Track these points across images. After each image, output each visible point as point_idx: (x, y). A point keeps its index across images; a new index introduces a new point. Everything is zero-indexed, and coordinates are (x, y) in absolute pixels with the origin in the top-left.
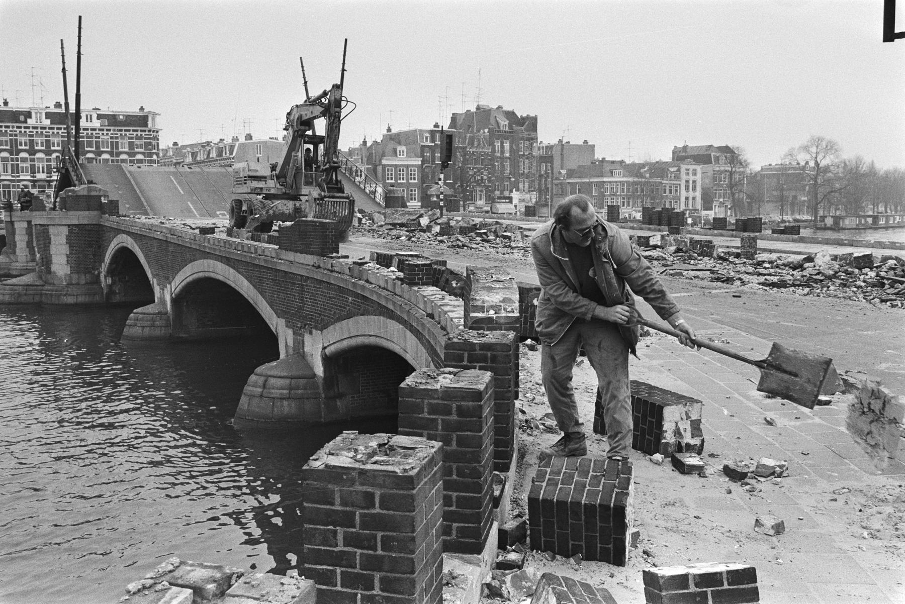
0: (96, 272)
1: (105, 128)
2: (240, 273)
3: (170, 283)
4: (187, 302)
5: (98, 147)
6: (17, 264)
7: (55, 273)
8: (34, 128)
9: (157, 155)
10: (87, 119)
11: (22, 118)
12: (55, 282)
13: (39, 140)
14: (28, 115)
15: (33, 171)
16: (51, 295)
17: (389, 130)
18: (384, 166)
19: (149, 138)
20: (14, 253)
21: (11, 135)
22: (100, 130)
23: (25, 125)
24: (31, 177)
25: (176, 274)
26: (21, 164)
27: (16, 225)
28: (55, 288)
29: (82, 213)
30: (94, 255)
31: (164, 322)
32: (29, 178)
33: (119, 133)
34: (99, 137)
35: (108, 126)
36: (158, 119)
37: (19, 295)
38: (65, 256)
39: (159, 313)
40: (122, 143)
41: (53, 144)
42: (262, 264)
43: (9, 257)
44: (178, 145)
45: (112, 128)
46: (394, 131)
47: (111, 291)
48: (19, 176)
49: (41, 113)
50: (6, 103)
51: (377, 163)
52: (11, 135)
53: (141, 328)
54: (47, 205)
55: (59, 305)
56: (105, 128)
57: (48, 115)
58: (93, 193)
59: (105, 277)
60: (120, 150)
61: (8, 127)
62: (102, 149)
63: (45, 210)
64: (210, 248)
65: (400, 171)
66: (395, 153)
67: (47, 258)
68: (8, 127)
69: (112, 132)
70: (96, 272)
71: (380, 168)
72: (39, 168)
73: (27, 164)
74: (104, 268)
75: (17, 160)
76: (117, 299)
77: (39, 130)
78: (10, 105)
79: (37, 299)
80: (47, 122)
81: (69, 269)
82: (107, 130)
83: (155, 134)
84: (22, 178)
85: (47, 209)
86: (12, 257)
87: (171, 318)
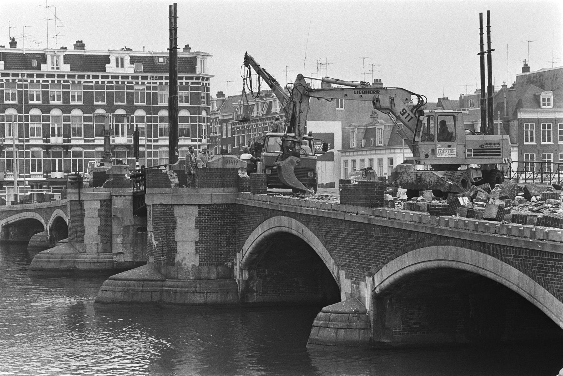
0: (230, 264)
1: (140, 75)
2: (506, 261)
3: (372, 275)
4: (391, 300)
5: (130, 101)
6: (85, 256)
7: (179, 264)
8: (49, 76)
9: (207, 110)
10: (117, 62)
11: (34, 63)
12: (180, 276)
13: (55, 92)
14: (106, 59)
15: (47, 133)
16: (175, 292)
17: (526, 68)
18: (521, 121)
19: (198, 88)
20: (82, 241)
21: (20, 86)
22: (133, 78)
23: (39, 72)
24: (44, 141)
25: (384, 264)
26: (32, 125)
27: (86, 205)
28: (180, 284)
29: (215, 190)
30: (228, 243)
31: (363, 323)
32: (41, 142)
33: (158, 81)
34: (132, 88)
35: (145, 72)
36: (208, 60)
37: (135, 292)
38: (194, 244)
39: (355, 312)
40: (161, 95)
41: (73, 97)
42: (548, 250)
43: (73, 247)
44: (223, 96)
45: (149, 75)
46: (534, 69)
47: (247, 289)
48: (28, 141)
49: (58, 56)
50: (13, 44)
51: (511, 116)
52: (20, 86)
53: (334, 331)
54: (172, 180)
55: (185, 304)
56: (140, 75)
57: (68, 59)
58: (229, 166)
59: (241, 270)
60: (160, 104)
61: (83, 77)
62: (135, 104)
63: (171, 187)
64: (451, 232)
65: (544, 127)
66: (536, 102)
67: (169, 245)
68: (16, 75)
69: (149, 80)
70: (230, 264)
71: (514, 125)
72: (53, 129)
73: (39, 125)
74: (240, 260)
75: (27, 119)
76: (254, 298)
77: (56, 79)
78: (18, 46)
79: (156, 297)
80: (65, 69)
81: (198, 259)
82: (143, 78)
83: (205, 82)
84: (31, 143)
85: (173, 185)
86: (77, 247)
87: (372, 318)
